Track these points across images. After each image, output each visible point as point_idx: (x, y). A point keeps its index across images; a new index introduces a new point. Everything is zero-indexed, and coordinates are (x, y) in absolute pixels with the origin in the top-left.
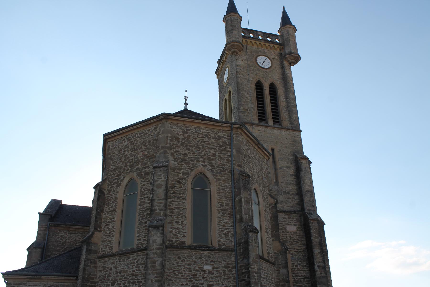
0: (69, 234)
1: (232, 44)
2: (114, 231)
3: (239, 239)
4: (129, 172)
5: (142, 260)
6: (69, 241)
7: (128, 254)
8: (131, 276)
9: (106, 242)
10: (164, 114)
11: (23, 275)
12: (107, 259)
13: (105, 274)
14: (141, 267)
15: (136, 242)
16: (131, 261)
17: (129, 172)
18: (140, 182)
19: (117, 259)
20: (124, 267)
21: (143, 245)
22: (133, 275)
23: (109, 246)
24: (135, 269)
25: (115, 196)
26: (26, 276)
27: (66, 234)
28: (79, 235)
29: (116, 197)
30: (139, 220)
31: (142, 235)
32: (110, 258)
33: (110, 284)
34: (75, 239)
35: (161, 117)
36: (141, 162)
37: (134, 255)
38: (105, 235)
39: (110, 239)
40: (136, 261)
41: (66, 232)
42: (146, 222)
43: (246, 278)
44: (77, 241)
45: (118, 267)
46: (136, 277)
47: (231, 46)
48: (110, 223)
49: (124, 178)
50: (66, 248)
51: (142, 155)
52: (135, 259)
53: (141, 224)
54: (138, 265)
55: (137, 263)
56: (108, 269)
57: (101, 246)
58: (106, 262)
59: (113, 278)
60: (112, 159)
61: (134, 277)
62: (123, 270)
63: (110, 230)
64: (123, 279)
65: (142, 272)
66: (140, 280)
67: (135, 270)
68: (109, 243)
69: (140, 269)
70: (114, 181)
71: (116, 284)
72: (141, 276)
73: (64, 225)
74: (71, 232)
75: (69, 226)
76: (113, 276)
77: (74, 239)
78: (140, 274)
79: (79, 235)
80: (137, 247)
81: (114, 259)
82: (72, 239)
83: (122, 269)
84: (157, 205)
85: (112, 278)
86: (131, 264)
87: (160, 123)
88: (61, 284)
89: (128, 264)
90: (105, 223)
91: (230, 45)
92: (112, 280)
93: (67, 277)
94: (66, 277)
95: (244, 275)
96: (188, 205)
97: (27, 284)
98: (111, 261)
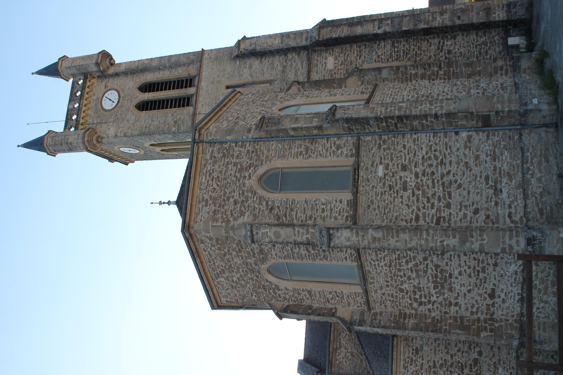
1: (87, 144)
2: (336, 292)
6: (350, 348)
8: (391, 268)
9: (349, 301)
10: (183, 231)
12: (371, 299)
13: (390, 300)
14: (380, 256)
15: (349, 262)
18: (272, 260)
19: (371, 286)
20: (380, 277)
24: (382, 264)
30: (321, 259)
33: (401, 294)
35: (187, 235)
37: (366, 265)
41: (339, 353)
43: (394, 122)
44: (349, 338)
47: (89, 144)
48: (325, 297)
49: (267, 281)
52: (371, 264)
54: (377, 260)
57: (355, 307)
58: (374, 301)
61: (393, 264)
64: (396, 278)
66: (397, 256)
67: (384, 263)
68: (351, 297)
69: (383, 257)
71: (402, 287)
72: (392, 255)
74: (338, 346)
75: (331, 350)
76: (392, 291)
78: (390, 257)
84: (302, 237)
88: (402, 356)
89: (377, 273)
92: (397, 293)
96: (300, 197)
98: (373, 294)
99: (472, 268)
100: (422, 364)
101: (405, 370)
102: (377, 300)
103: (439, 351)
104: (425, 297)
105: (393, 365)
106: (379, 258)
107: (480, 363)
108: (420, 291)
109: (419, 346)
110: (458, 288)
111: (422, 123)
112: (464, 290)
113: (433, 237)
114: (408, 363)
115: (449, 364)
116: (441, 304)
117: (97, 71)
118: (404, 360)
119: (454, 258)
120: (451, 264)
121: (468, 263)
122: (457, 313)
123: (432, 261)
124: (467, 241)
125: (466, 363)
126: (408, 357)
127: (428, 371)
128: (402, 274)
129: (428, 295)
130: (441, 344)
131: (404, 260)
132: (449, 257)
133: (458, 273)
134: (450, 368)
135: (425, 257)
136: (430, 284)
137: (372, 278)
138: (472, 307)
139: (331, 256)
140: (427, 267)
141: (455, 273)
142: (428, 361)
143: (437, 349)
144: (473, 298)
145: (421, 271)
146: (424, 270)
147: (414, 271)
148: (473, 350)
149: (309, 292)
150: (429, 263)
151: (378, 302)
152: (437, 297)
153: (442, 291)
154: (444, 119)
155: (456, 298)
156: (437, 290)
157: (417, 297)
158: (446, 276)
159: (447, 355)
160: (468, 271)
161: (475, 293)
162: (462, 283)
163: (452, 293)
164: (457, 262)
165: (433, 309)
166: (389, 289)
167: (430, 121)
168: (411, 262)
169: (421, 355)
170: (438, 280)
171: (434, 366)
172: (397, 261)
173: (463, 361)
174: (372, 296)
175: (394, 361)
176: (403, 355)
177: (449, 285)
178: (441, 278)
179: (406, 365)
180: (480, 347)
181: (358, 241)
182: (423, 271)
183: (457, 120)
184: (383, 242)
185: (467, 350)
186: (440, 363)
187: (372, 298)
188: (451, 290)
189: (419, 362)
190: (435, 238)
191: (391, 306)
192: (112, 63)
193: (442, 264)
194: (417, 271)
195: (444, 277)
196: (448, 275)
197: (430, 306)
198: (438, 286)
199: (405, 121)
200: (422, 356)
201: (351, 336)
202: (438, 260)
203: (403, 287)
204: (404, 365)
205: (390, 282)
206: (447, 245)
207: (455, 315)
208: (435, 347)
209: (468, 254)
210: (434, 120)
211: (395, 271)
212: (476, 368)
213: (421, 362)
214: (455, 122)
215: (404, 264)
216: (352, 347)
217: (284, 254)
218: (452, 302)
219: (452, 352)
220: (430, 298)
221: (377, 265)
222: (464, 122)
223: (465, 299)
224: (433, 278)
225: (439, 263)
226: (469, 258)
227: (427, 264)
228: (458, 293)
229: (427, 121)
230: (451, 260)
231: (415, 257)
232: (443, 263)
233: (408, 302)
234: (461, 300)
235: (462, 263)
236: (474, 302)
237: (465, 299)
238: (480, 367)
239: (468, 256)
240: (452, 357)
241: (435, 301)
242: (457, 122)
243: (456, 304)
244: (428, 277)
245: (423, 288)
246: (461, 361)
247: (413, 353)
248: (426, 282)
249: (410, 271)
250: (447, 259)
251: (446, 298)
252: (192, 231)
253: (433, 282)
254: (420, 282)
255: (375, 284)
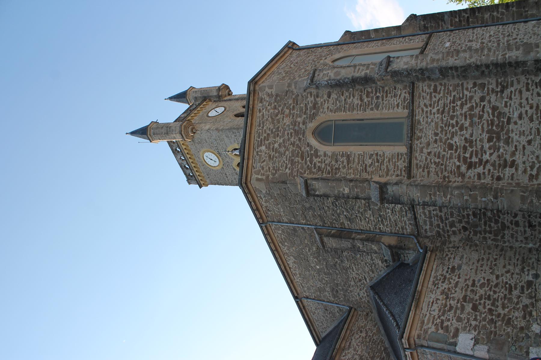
0: (349, 350)
1: (183, 127)
2: (377, 154)
3: (420, 30)
4: (304, 137)
5: (426, 98)
6: (360, 350)
7: (414, 122)
8: (444, 115)
9: (389, 166)
10: (250, 83)
11: (412, 302)
12: (414, 162)
13: (435, 163)
14: (434, 99)
15: (400, 110)
16: (424, 118)
17: (304, 137)
18: (322, 115)
19: (417, 142)
20: (430, 129)
21: (406, 98)
22: (443, 112)
23: (396, 160)
24: (435, 110)
25: (329, 157)
26: (412, 309)
27: (348, 353)
28: (355, 338)
29: (330, 156)
30: (372, 109)
31: (393, 103)
32: (413, 156)
33: (450, 152)
34: (359, 342)
35: (252, 88)
36: (296, 118)
37: (417, 113)
38: (379, 169)
39: (387, 160)
40: (425, 109)
41: (345, 353)
42: (378, 98)
43: (466, 16)
44: (362, 340)
45: (428, 140)
46: (447, 107)
47: (184, 129)
48: (364, 163)
49: (308, 145)
50: (369, 355)
51: (288, 118)
52: (423, 111)
53: (377, 107)
54: (430, 105)
55: (429, 107)
56: (429, 157)
57: (394, 177)
58: (417, 164)
59: (443, 148)
60: (277, 170)
61: (447, 109)
62: (434, 130)
63: (373, 162)
64: (447, 128)
65: (441, 97)
66: (452, 98)
67: (438, 108)
68: (392, 161)
69: (437, 101)
70: (308, 163)
71: (451, 142)
72: (447, 97)
73: (333, 352)
74: (347, 347)
75: (337, 346)
76: (440, 149)
77: (359, 344)
78: (444, 99)
79: (355, 338)
80: (407, 109)
81: (415, 150)
82: (357, 347)
83: (433, 132)
84: (361, 73)
85: (442, 150)
86: (427, 117)
87: (257, 93)
88: (433, 273)
89: (427, 123)
90: (363, 172)
91: (183, 130)
92: (444, 151)
93: (425, 260)
94: (425, 262)
95: (462, 19)
96: (355, 150)
97: (425, 314)
98: (417, 155)
99: (534, 108)
100: (457, 282)
101: (435, 287)
102: (421, 163)
103: (482, 270)
104: (476, 155)
105: (421, 276)
106: (432, 103)
107: (535, 285)
108: (471, 147)
109: (456, 265)
110: (516, 138)
111: (493, 16)
112: (523, 140)
113: (495, 52)
114: (440, 280)
115: (494, 284)
116: (493, 165)
117: (215, 96)
118: (436, 277)
119: (515, 96)
120: (510, 105)
121: (530, 102)
122: (512, 179)
123: (489, 102)
124: (532, 51)
125: (516, 285)
126: (442, 275)
127: (464, 289)
128: (454, 122)
129: (480, 152)
130: (485, 265)
131: (459, 103)
132: (509, 94)
133: (518, 115)
134: (493, 288)
135: (483, 96)
136: (484, 134)
137: (421, 130)
138: (532, 168)
139: (383, 103)
140: (483, 111)
141: (515, 116)
142: (466, 280)
143: (480, 268)
144: (533, 153)
145: (476, 117)
146: (479, 114)
147: (468, 117)
148: (526, 273)
149: (348, 157)
150: (486, 105)
151: (421, 166)
152: (491, 154)
153: (497, 144)
154: (514, 9)
155: (513, 154)
156: (492, 144)
157: (467, 155)
158: (503, 122)
159: (491, 275)
160: (530, 112)
161: (536, 145)
162: (522, 130)
163: (508, 146)
164: (518, 102)
165: (484, 173)
166: (436, 146)
167: (501, 12)
168: (466, 104)
169: (458, 273)
170: (494, 128)
171: (473, 285)
172: (452, 105)
173: (512, 282)
174: (416, 158)
175: (423, 272)
176: (435, 273)
177: (506, 134)
178: (498, 126)
179: (437, 282)
180: (537, 271)
181: (417, 63)
182: (478, 116)
183: (527, 9)
184: (441, 62)
185: (519, 272)
186: (480, 283)
187: (415, 161)
188: (507, 142)
189: (454, 280)
190: (497, 53)
191: (435, 172)
192: (230, 93)
193: (500, 105)
194: (472, 116)
195: (501, 124)
196: (505, 120)
197: (480, 170)
198: (493, 137)
199: (477, 14)
200: (459, 275)
201: (365, 338)
202: (496, 101)
203: (453, 142)
204: (434, 282)
205: (440, 135)
206: (509, 57)
207: (510, 181)
208: (477, 267)
209: (531, 89)
210: (505, 11)
211: (447, 118)
212: (530, 291)
213: (457, 280)
214: (525, 11)
215: (458, 108)
216: (363, 350)
217: (336, 106)
218: (508, 160)
219: (499, 273)
220: (482, 156)
221: (429, 112)
222: (534, 12)
223: (524, 155)
224: (488, 126)
225: (498, 104)
226: (532, 94)
227: (484, 105)
228: (516, 146)
229: (498, 12)
230: (511, 99)
231: (471, 98)
232: (502, 104)
233: (455, 163)
234: (519, 158)
235: (524, 101)
236: (534, 160)
237: (524, 155)
238: (536, 289)
239: (531, 91)
240: (497, 277)
241: (487, 161)
242: (528, 11)
243: (513, 164)
244: (483, 124)
245: (476, 141)
246: (509, 282)
247: (447, 272)
248: (480, 132)
249: (463, 117)
250: (507, 98)
251: (501, 154)
252: (257, 88)
253: (488, 132)
254: (473, 133)
255: (422, 139)
